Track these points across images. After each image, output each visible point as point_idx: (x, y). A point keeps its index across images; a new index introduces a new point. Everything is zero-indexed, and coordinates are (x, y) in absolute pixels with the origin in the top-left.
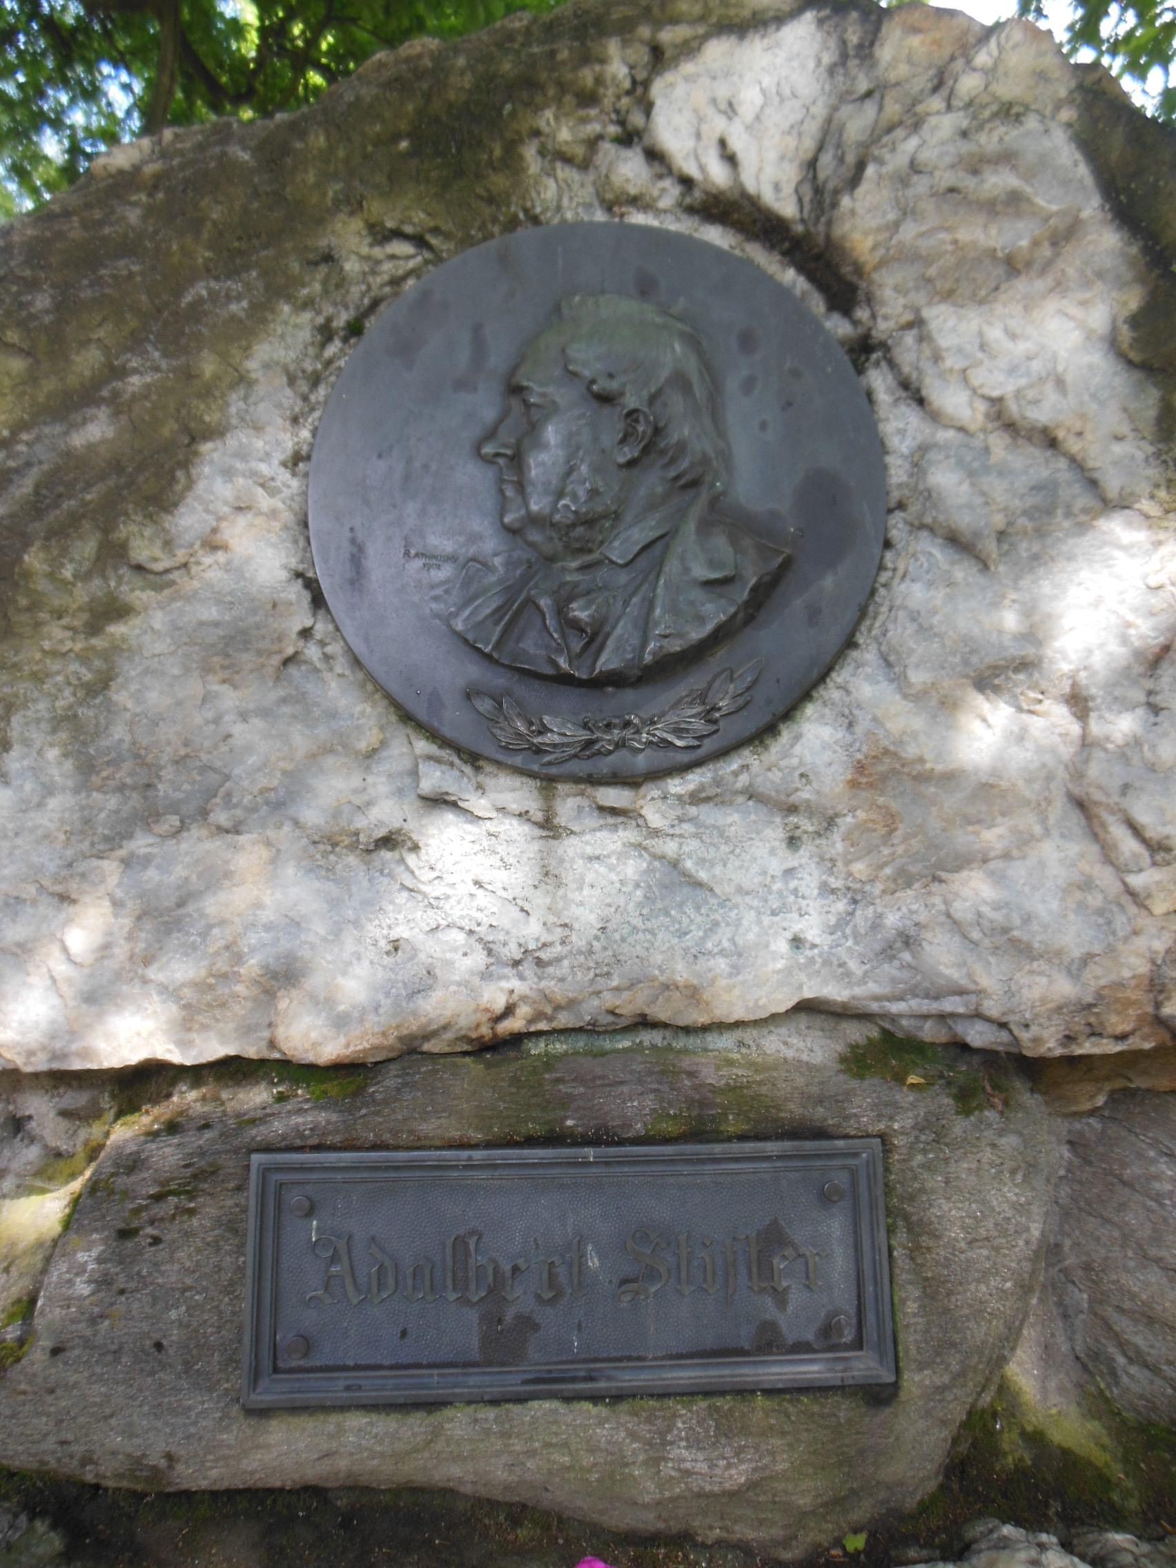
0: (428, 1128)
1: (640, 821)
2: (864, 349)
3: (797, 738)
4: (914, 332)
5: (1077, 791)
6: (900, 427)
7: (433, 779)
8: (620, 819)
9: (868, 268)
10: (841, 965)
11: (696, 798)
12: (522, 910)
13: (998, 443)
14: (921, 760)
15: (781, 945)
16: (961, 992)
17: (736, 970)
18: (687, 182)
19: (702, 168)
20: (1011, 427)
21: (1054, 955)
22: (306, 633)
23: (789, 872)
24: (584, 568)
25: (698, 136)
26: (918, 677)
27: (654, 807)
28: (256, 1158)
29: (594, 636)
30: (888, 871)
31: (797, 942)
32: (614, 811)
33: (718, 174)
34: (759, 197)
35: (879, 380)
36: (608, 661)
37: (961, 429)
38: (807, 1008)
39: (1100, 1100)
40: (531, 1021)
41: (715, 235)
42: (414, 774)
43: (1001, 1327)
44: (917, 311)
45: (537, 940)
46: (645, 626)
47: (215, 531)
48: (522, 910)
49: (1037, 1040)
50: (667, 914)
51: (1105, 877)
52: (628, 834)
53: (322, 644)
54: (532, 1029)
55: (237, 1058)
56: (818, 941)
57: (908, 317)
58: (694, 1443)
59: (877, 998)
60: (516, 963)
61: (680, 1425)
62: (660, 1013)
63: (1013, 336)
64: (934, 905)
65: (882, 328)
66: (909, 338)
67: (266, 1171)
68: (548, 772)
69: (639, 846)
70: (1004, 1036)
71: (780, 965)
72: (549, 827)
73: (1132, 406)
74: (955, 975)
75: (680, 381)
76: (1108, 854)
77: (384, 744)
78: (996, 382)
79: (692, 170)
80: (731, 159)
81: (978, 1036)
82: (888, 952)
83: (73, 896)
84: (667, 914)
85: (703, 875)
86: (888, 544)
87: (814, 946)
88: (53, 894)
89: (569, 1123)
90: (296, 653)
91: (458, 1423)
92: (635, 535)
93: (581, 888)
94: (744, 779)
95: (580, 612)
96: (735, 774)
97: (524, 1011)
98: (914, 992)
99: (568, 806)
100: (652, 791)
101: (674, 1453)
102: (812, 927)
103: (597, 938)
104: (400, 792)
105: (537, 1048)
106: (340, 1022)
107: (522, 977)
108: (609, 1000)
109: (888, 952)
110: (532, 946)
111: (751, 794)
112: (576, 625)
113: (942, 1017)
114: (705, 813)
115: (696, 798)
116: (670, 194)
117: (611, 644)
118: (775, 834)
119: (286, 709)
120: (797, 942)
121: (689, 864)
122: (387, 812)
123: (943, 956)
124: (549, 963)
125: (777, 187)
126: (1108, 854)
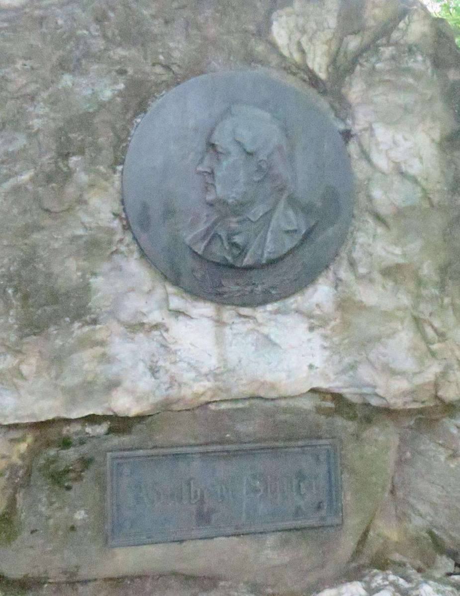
0: (176, 439)
1: (255, 320)
2: (347, 135)
3: (316, 290)
4: (369, 132)
5: (415, 314)
6: (360, 169)
7: (176, 302)
8: (247, 319)
9: (354, 105)
10: (327, 375)
11: (277, 312)
12: (209, 355)
13: (396, 179)
14: (362, 302)
15: (306, 368)
16: (368, 385)
17: (289, 377)
18: (282, 56)
19: (291, 54)
20: (403, 174)
21: (403, 374)
22: (121, 241)
23: (309, 340)
24: (238, 222)
25: (290, 39)
26: (362, 270)
27: (260, 313)
28: (109, 454)
29: (242, 250)
30: (346, 341)
31: (311, 367)
32: (245, 316)
33: (297, 57)
34: (313, 70)
35: (353, 148)
36: (248, 260)
37: (383, 173)
38: (314, 391)
39: (412, 423)
40: (212, 397)
41: (291, 82)
42: (166, 300)
43: (438, 565)
44: (371, 124)
45: (215, 366)
46: (262, 245)
47: (81, 196)
48: (209, 355)
49: (395, 403)
50: (264, 356)
51: (423, 345)
52: (250, 325)
53: (128, 245)
54: (212, 400)
55: (94, 415)
56: (318, 366)
57: (367, 125)
58: (273, 548)
59: (337, 387)
60: (206, 375)
61: (268, 543)
62: (262, 394)
63: (406, 139)
64: (362, 355)
65: (356, 129)
66: (367, 134)
67: (114, 458)
68: (219, 297)
69: (253, 330)
70: (385, 401)
71: (305, 375)
72: (219, 323)
73: (445, 170)
74: (368, 379)
75: (279, 148)
76: (424, 337)
77: (154, 288)
78: (398, 154)
79: (286, 53)
80: (303, 52)
81: (374, 402)
82: (344, 371)
83: (24, 352)
84: (264, 356)
85: (278, 341)
86: (353, 216)
87: (317, 368)
88: (14, 351)
89: (228, 435)
90: (116, 250)
91: (189, 547)
92: (259, 210)
93: (231, 346)
94: (294, 306)
95: (238, 239)
96: (292, 304)
97: (209, 393)
98: (351, 386)
99: (228, 313)
100: (260, 309)
101: (266, 552)
102: (318, 362)
103: (237, 365)
104: (160, 308)
105: (212, 407)
106: (138, 400)
107: (209, 381)
108: (242, 389)
109: (344, 371)
110: (212, 369)
111: (297, 311)
112: (235, 245)
113: (361, 395)
114: (280, 318)
115: (277, 312)
116: (274, 60)
117: (248, 254)
118: (303, 326)
119: (113, 273)
120: (311, 367)
121: (272, 337)
122: (156, 316)
123: (365, 373)
124: (219, 375)
125: (320, 68)
126: (424, 337)
